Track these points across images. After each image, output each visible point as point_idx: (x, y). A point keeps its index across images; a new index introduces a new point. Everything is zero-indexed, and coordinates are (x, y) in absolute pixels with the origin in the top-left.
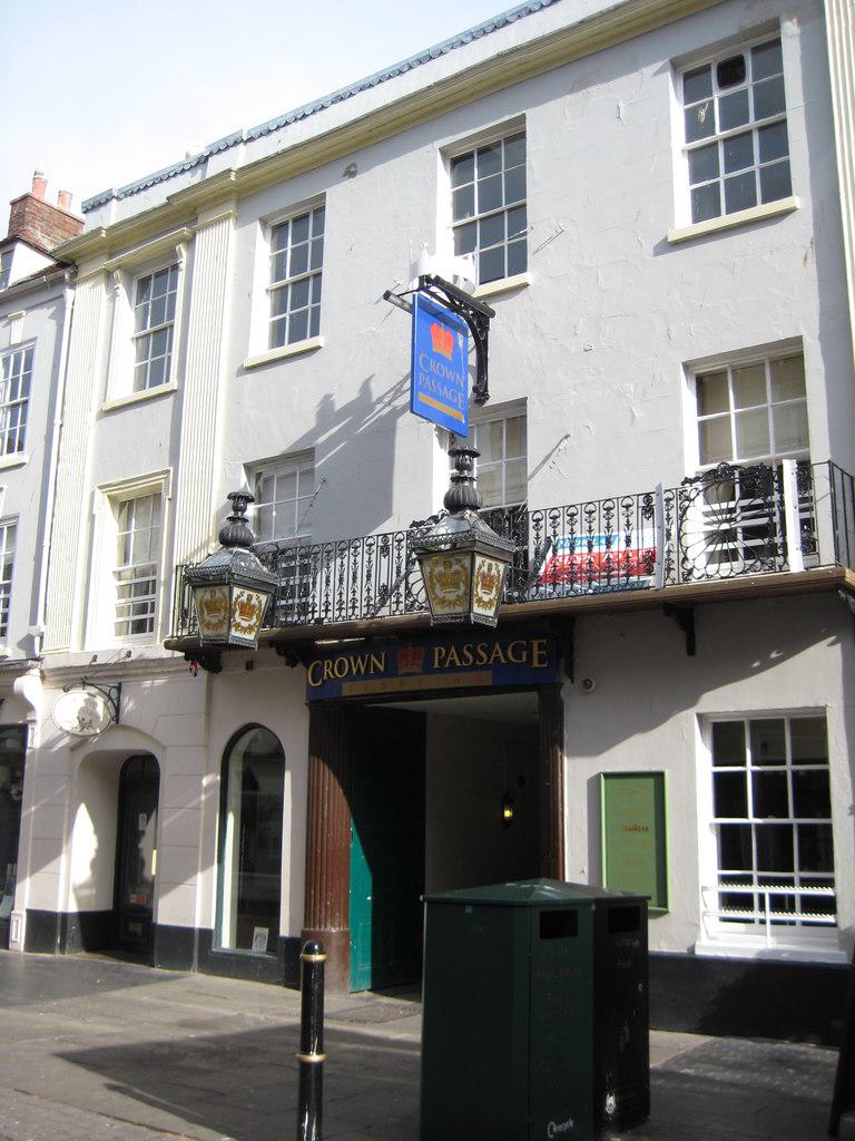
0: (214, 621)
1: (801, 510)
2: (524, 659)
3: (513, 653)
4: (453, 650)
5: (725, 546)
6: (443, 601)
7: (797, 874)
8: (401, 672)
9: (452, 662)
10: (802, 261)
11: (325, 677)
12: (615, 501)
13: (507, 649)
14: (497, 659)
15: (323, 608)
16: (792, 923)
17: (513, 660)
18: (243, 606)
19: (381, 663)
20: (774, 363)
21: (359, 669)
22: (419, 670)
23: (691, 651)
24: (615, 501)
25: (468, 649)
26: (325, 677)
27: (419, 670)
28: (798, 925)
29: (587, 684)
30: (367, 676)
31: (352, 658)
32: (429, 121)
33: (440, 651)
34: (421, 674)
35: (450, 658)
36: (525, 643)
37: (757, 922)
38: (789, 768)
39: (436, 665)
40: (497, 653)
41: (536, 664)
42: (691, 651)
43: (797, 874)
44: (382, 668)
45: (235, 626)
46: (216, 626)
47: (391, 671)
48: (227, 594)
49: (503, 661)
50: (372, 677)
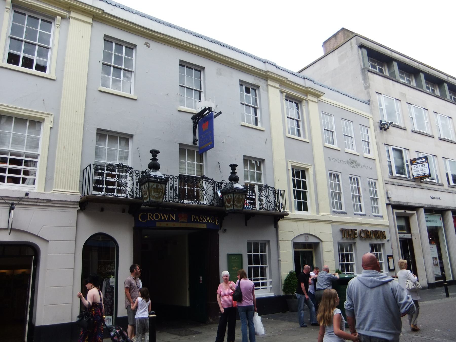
0: (156, 196)
1: (426, 218)
2: (214, 222)
3: (155, 216)
4: (197, 216)
5: (120, 188)
6: (153, 197)
7: (260, 278)
8: (180, 221)
9: (197, 220)
10: (265, 143)
11: (149, 219)
12: (139, 171)
13: (210, 218)
14: (208, 221)
15: (169, 197)
16: (259, 289)
17: (156, 219)
18: (227, 200)
19: (165, 216)
20: (30, 121)
21: (165, 218)
22: (186, 221)
23: (246, 225)
24: (139, 171)
25: (201, 217)
26: (149, 219)
27: (186, 221)
28: (261, 289)
29: (225, 231)
30: (168, 221)
31: (161, 214)
32: (292, 90)
33: (193, 216)
34: (187, 223)
35: (196, 219)
36: (214, 217)
37: (261, 289)
38: (260, 253)
39: (192, 221)
40: (208, 219)
41: (216, 224)
42: (246, 225)
43: (260, 278)
44: (167, 219)
45: (152, 197)
46: (157, 198)
47: (177, 220)
48: (232, 196)
49: (210, 222)
50: (170, 221)
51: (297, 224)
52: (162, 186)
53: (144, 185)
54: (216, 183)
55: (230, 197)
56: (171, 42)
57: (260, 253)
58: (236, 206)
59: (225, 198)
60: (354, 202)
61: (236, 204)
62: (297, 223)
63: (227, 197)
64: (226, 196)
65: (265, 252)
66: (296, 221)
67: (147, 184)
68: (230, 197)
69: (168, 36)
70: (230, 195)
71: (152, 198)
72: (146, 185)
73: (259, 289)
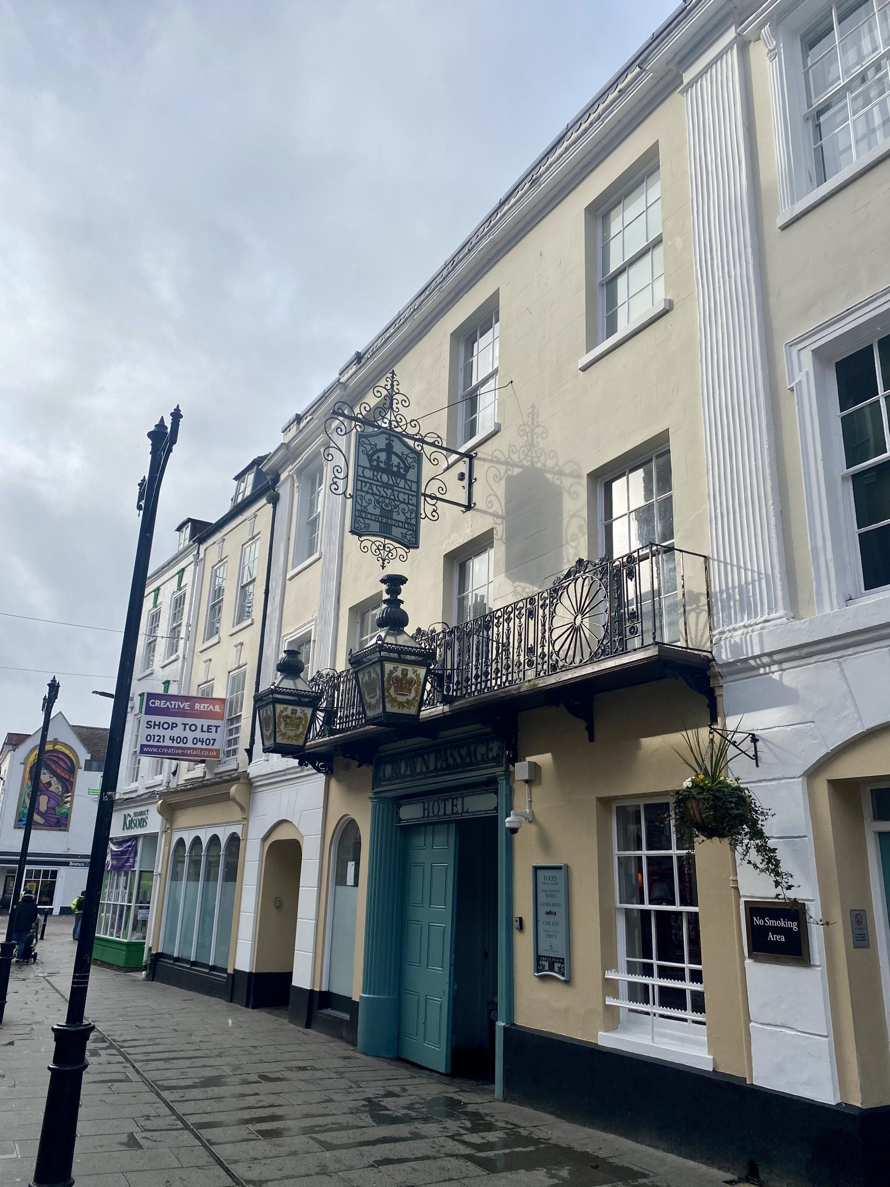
16: (685, 1020)
18: (398, 681)
42: (591, 739)
43: (687, 966)
51: (842, 670)
52: (418, 673)
53: (266, 708)
54: (499, 613)
55: (373, 675)
56: (878, 295)
57: (674, 852)
58: (394, 700)
59: (363, 679)
60: (767, 47)
61: (393, 695)
62: (840, 664)
63: (366, 678)
64: (364, 675)
65: (623, 861)
66: (838, 654)
67: (271, 706)
68: (373, 675)
69: (447, 304)
70: (374, 670)
71: (280, 738)
72: (270, 708)
73: (685, 1020)
